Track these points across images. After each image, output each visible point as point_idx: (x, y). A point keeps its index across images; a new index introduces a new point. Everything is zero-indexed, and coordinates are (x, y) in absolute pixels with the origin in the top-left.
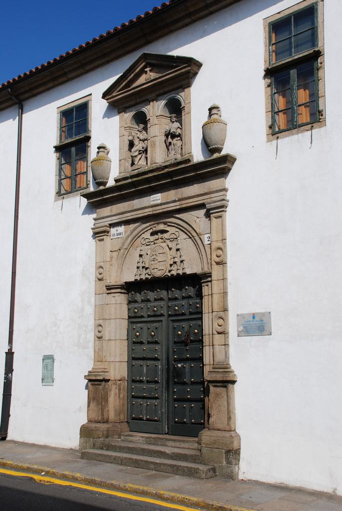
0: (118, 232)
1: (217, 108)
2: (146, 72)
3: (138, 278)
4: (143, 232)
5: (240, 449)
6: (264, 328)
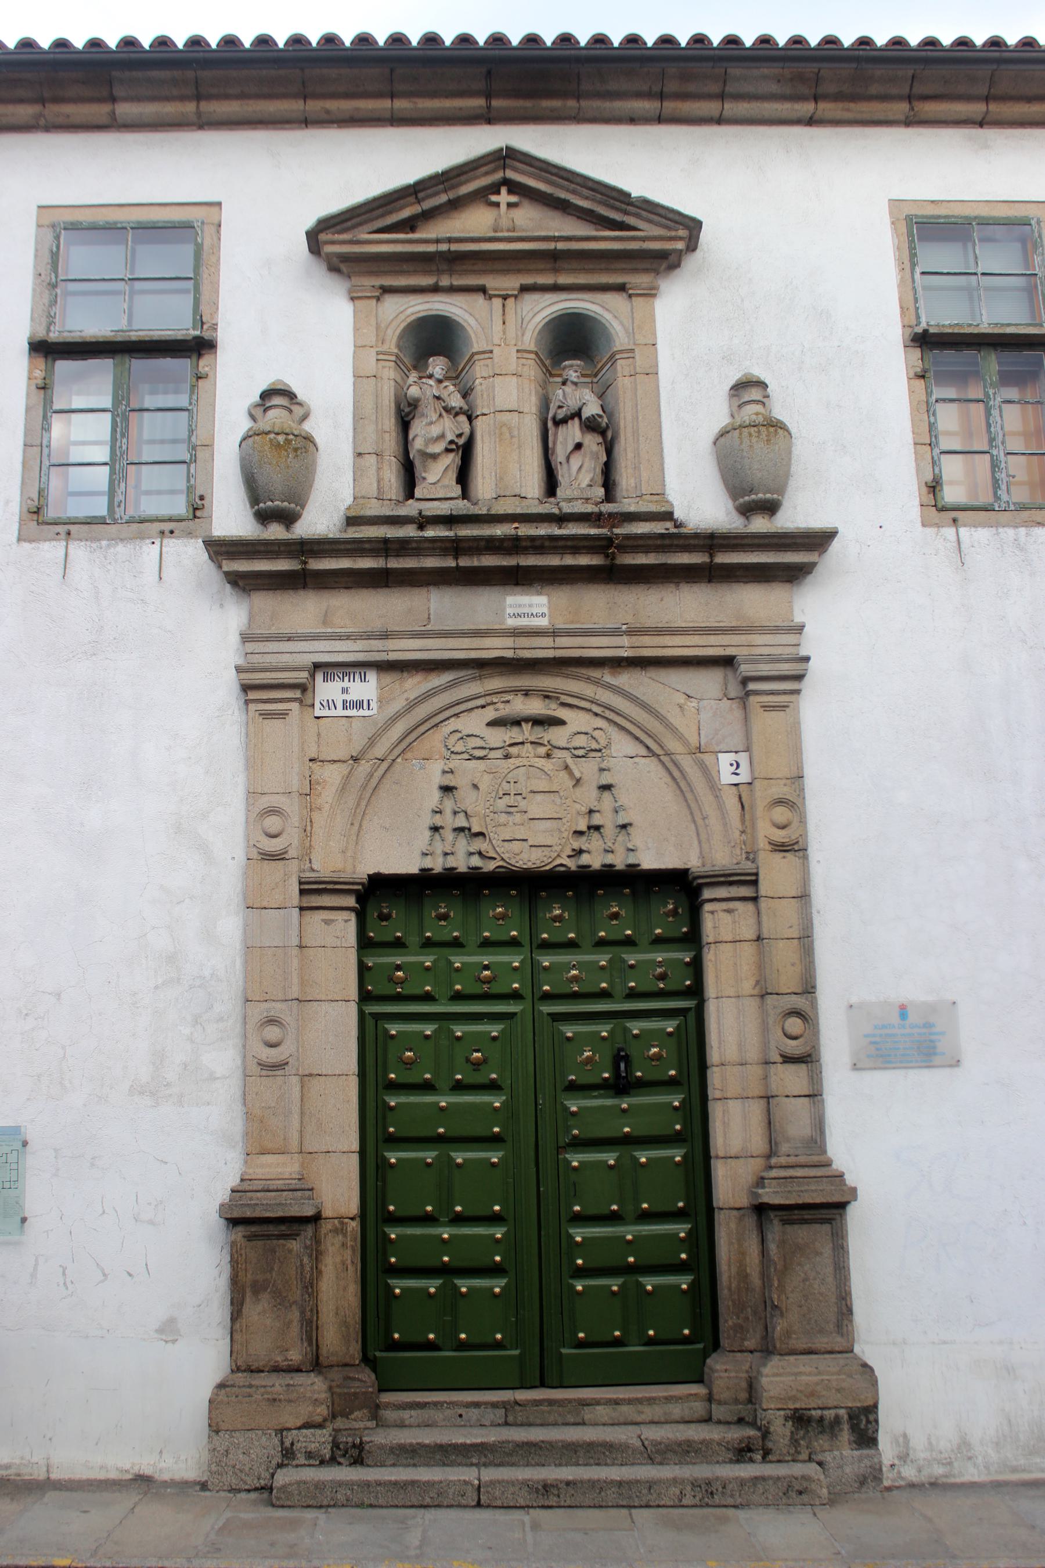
0: (348, 697)
1: (762, 385)
3: (437, 865)
4: (456, 709)
5: (875, 1406)
6: (935, 1048)
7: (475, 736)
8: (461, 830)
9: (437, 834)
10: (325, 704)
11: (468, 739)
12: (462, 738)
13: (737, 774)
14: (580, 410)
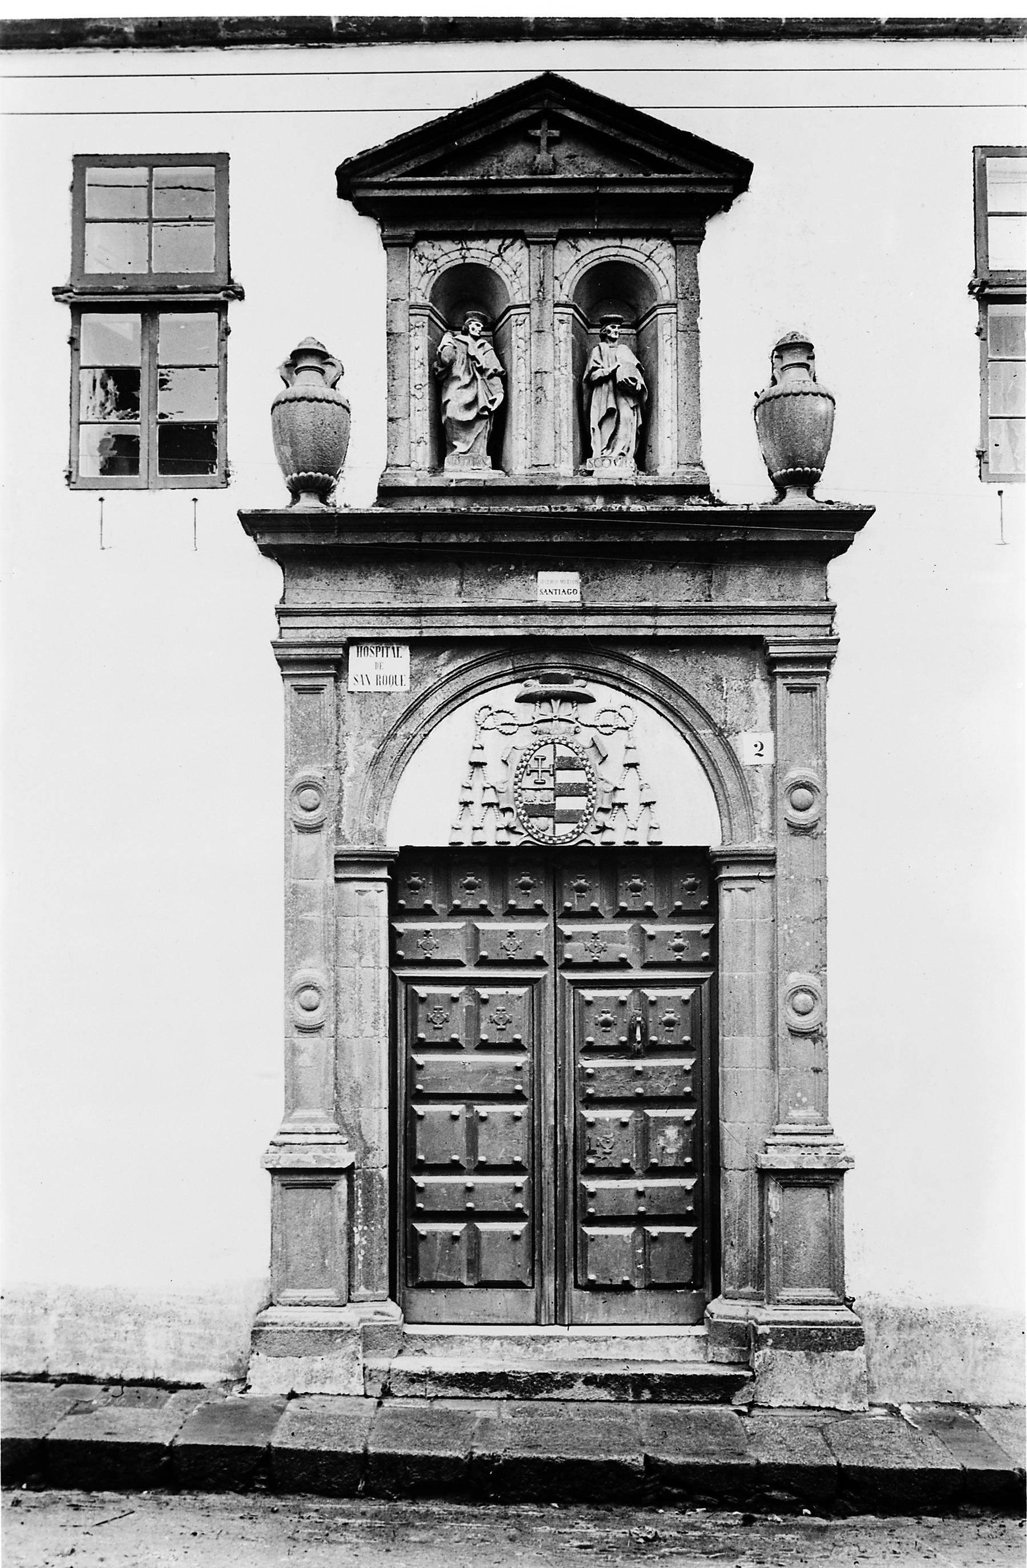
0: (381, 673)
1: (808, 347)
2: (535, 141)
7: (505, 712)
8: (490, 805)
9: (466, 808)
10: (359, 679)
11: (499, 714)
12: (492, 714)
13: (761, 755)
14: (614, 371)
